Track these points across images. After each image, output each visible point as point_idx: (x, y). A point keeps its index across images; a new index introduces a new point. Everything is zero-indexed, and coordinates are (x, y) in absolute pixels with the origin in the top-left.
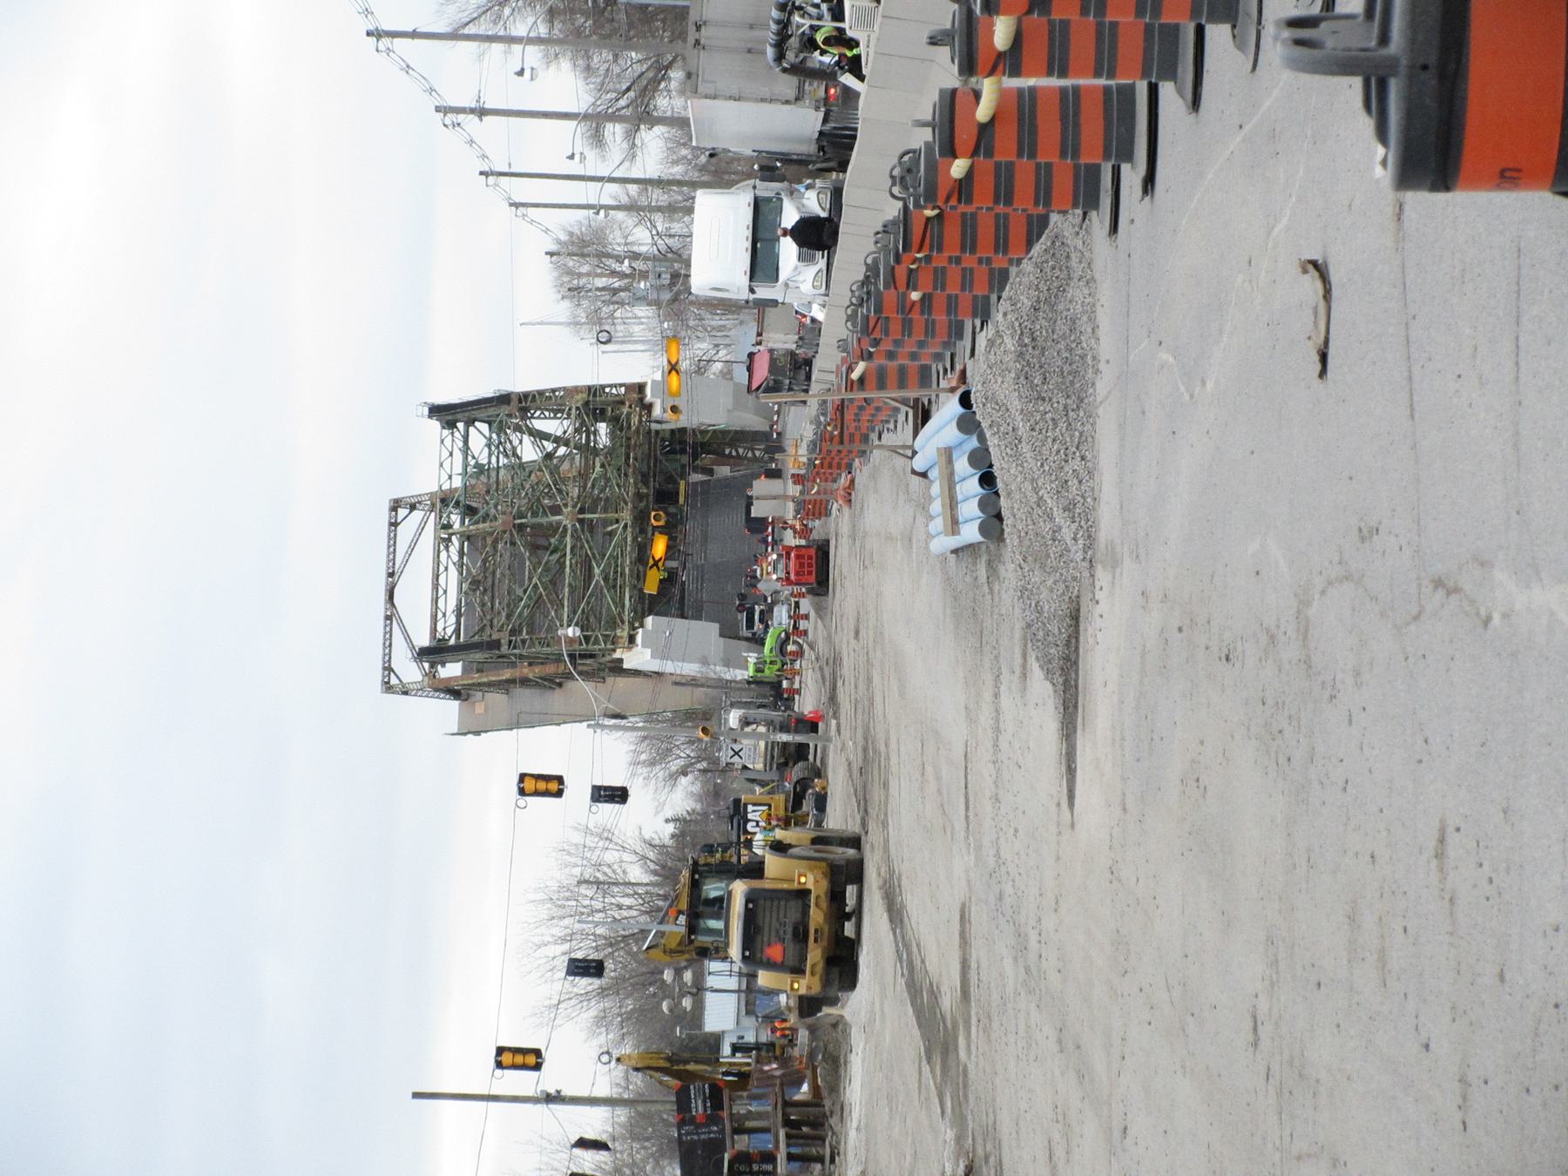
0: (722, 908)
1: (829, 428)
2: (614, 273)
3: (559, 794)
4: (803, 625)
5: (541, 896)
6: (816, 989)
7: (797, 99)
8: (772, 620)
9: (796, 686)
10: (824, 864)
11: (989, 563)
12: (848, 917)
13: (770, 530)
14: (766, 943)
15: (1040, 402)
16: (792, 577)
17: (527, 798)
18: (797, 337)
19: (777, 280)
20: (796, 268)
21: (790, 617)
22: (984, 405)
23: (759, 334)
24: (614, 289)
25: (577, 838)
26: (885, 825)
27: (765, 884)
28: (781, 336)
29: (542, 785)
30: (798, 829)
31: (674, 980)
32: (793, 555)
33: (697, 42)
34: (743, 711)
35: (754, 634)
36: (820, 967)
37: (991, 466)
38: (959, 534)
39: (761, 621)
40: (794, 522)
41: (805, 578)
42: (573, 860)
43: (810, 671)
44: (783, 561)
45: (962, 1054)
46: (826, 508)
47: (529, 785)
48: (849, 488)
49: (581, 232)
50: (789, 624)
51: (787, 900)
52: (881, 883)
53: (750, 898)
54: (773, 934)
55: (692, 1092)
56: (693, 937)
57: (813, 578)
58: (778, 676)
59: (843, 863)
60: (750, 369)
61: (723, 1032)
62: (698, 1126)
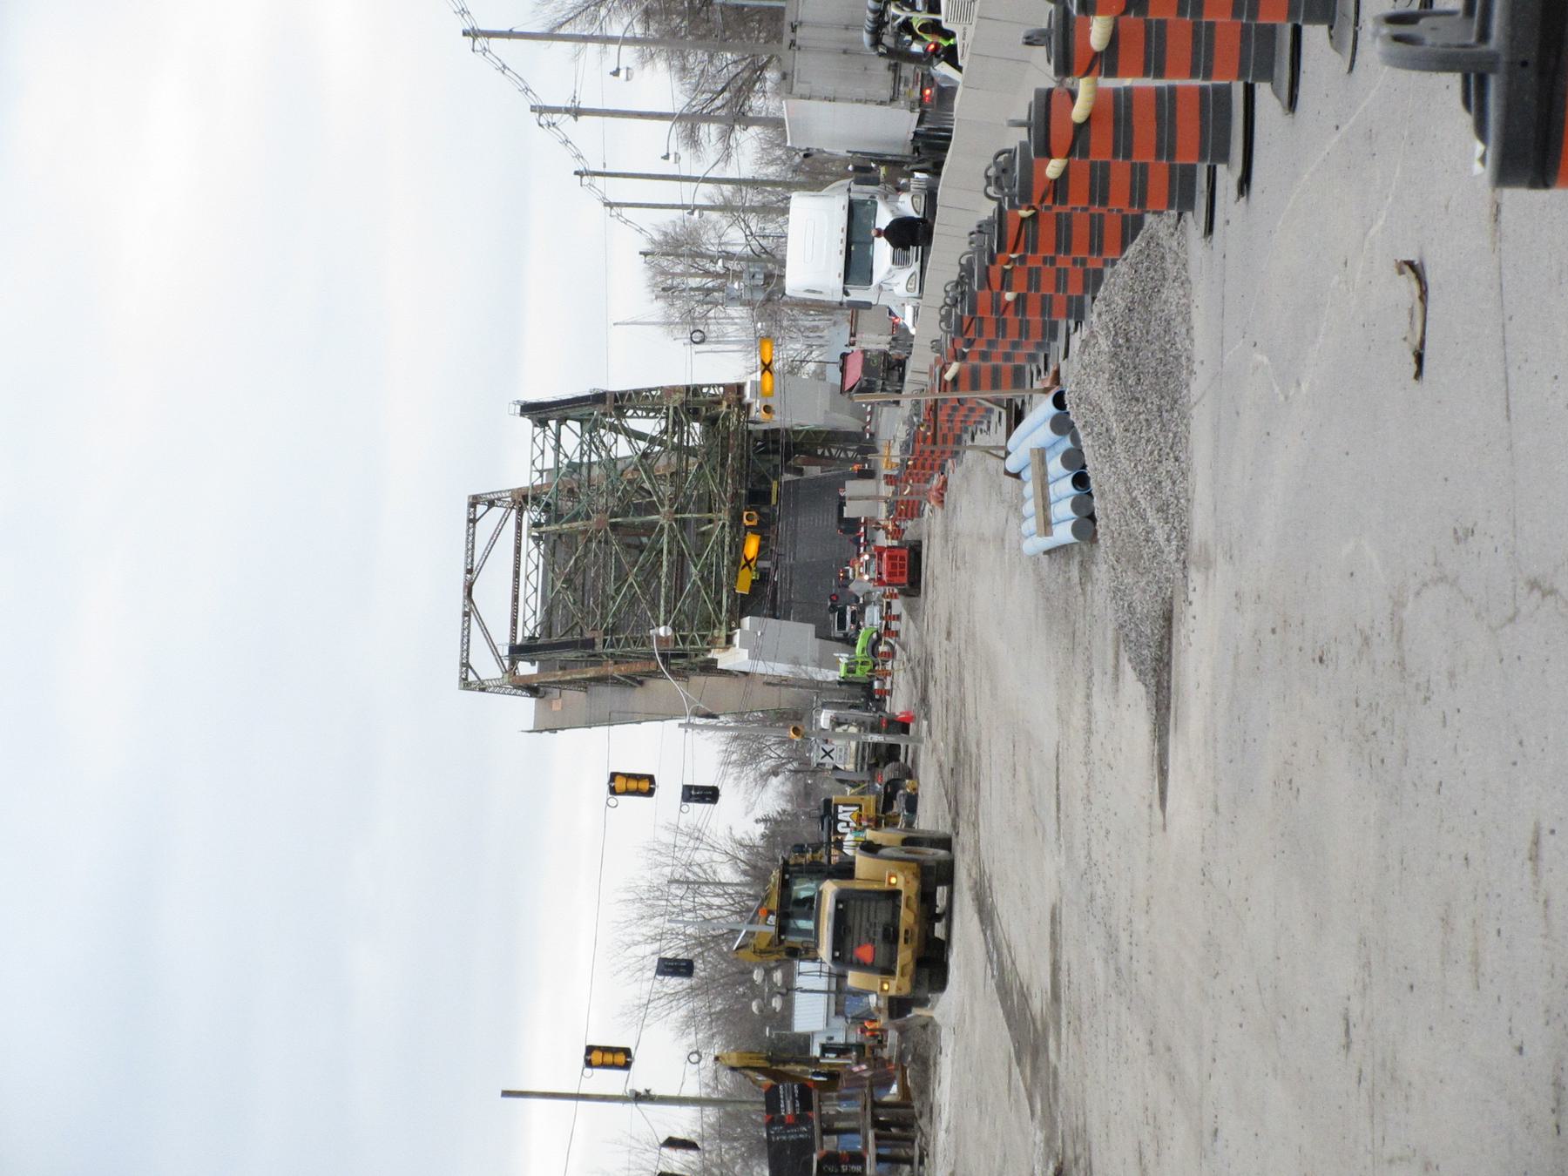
0: (811, 908)
1: (922, 429)
2: (707, 273)
3: (650, 793)
4: (894, 625)
5: (631, 896)
6: (906, 989)
7: (892, 100)
8: (864, 620)
9: (888, 687)
10: (914, 865)
11: (1082, 563)
12: (938, 918)
13: (862, 530)
14: (855, 944)
15: (1134, 403)
16: (885, 578)
17: (618, 797)
18: (890, 338)
19: (871, 282)
20: (890, 271)
21: (882, 618)
22: (1078, 406)
23: (853, 335)
24: (708, 289)
25: (668, 838)
26: (975, 825)
27: (857, 885)
28: (874, 337)
29: (633, 785)
30: (888, 829)
31: (764, 980)
32: (885, 555)
33: (793, 43)
34: (834, 711)
35: (846, 635)
36: (911, 967)
37: (1084, 467)
38: (1052, 534)
39: (853, 621)
40: (887, 523)
41: (895, 580)
42: (663, 859)
43: (902, 672)
44: (875, 562)
45: (1052, 1056)
46: (919, 509)
47: (620, 784)
48: (942, 488)
49: (676, 233)
50: (881, 624)
51: (877, 902)
52: (971, 883)
53: (840, 899)
54: (863, 934)
55: (781, 1092)
56: (783, 937)
57: (905, 580)
58: (870, 677)
59: (934, 864)
60: (843, 370)
61: (813, 1033)
62: (787, 1127)
